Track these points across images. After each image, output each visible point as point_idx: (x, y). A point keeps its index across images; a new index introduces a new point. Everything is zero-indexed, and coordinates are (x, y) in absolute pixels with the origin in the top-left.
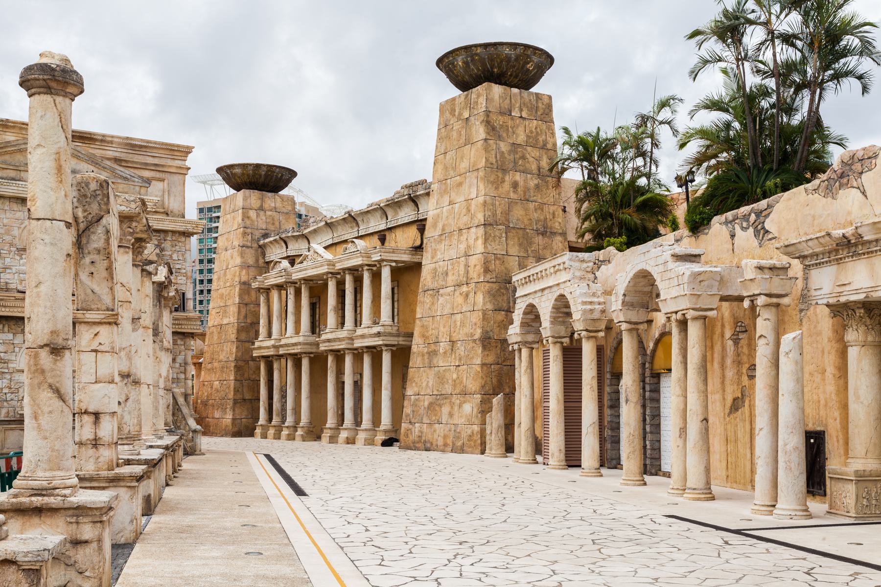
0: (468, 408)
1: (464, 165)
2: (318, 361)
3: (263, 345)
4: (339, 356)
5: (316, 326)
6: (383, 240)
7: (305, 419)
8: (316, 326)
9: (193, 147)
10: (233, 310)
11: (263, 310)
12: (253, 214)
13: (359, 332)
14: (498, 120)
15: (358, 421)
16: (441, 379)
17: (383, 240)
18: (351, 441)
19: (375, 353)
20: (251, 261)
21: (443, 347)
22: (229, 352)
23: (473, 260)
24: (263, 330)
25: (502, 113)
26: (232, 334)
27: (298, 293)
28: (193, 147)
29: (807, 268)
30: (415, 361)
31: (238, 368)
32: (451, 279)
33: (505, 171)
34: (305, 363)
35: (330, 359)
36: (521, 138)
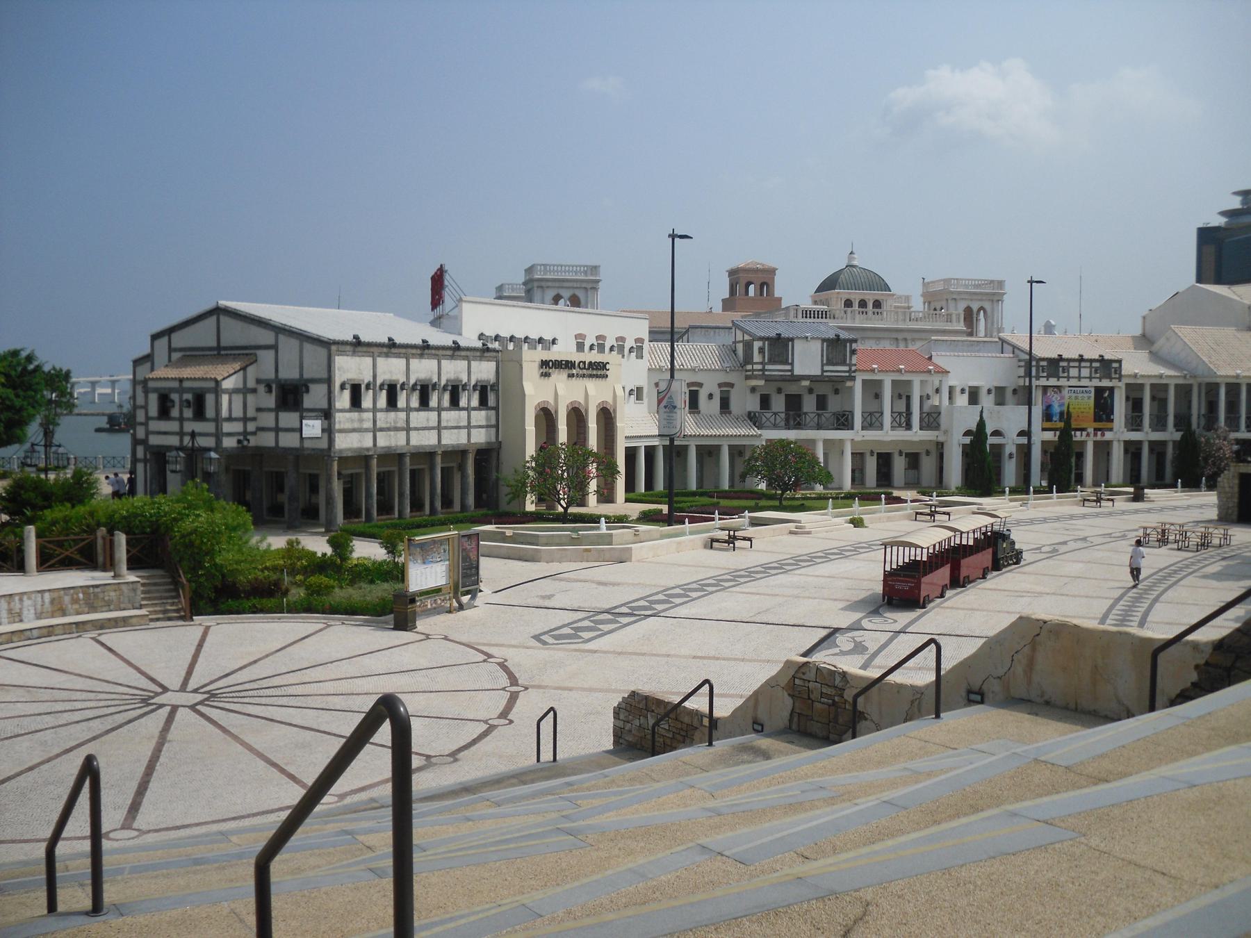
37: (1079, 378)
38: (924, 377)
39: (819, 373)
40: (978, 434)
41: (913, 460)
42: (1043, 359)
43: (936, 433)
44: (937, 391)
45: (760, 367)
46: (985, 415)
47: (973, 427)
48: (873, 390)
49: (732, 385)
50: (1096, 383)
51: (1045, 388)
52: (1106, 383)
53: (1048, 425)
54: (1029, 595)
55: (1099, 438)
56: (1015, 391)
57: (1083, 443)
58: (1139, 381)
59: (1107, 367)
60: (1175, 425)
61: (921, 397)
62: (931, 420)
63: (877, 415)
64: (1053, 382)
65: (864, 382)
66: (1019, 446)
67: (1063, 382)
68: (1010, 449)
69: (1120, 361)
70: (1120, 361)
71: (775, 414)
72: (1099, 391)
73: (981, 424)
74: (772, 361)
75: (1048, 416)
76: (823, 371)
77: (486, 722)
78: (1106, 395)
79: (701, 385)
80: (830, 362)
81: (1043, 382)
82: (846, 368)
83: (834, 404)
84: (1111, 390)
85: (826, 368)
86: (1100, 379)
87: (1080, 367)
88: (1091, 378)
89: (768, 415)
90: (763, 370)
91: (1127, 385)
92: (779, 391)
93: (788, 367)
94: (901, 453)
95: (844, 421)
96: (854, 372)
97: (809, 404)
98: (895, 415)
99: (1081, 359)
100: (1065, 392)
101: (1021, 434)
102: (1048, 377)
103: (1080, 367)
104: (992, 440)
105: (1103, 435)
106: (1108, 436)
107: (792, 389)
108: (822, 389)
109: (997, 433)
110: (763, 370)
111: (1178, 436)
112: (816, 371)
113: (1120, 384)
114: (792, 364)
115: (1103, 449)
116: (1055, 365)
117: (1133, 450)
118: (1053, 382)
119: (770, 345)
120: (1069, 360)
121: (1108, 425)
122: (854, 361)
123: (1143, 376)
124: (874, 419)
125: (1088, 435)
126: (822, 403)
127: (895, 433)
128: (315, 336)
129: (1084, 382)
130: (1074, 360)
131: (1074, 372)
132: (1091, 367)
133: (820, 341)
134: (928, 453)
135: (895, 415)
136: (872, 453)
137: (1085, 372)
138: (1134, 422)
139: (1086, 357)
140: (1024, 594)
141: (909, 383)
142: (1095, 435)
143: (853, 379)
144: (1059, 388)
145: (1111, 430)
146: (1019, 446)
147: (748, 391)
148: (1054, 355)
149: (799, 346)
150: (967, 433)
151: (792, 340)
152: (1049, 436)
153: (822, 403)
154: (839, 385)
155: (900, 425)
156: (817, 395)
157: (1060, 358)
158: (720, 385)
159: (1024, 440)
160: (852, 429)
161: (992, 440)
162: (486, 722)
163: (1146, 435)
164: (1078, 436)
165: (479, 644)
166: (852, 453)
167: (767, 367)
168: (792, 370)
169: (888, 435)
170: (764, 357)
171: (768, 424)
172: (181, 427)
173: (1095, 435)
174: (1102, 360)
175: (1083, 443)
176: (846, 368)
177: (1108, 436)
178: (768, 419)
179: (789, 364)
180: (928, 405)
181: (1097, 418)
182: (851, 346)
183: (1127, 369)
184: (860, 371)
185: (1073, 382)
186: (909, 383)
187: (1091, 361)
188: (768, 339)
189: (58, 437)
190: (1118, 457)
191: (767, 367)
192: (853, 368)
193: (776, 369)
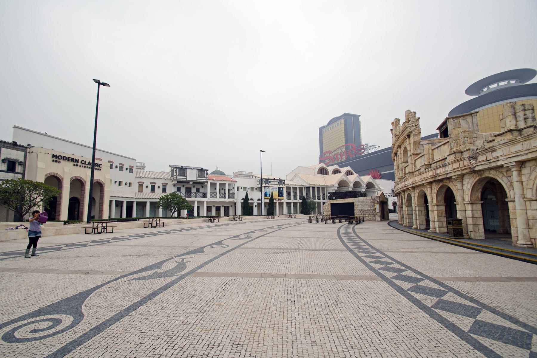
9: (360, 116)
28: (360, 116)
37: (274, 184)
38: (230, 183)
40: (246, 199)
41: (227, 209)
43: (233, 199)
44: (234, 188)
45: (175, 177)
46: (248, 193)
47: (244, 197)
48: (213, 185)
49: (167, 184)
50: (279, 186)
51: (265, 187)
52: (281, 186)
53: (266, 197)
54: (282, 251)
55: (280, 201)
57: (276, 203)
58: (290, 186)
59: (281, 181)
60: (300, 198)
61: (229, 190)
62: (232, 195)
63: (215, 194)
64: (267, 185)
66: (258, 203)
67: (269, 185)
68: (256, 204)
69: (284, 180)
70: (284, 180)
71: (201, 193)
72: (279, 188)
73: (247, 196)
74: (179, 175)
75: (266, 195)
76: (197, 179)
78: (281, 189)
79: (155, 183)
80: (199, 176)
82: (205, 179)
83: (202, 190)
84: (283, 188)
85: (198, 178)
86: (280, 185)
87: (274, 182)
88: (277, 185)
89: (199, 193)
90: (176, 178)
91: (287, 187)
92: (183, 186)
93: (186, 177)
94: (223, 206)
95: (205, 195)
96: (208, 180)
97: (194, 190)
98: (211, 194)
99: (274, 179)
101: (259, 200)
102: (265, 184)
103: (274, 182)
104: (250, 201)
105: (281, 201)
106: (282, 201)
107: (188, 186)
109: (251, 199)
110: (176, 178)
111: (301, 201)
112: (195, 179)
113: (285, 187)
114: (186, 176)
115: (281, 204)
116: (267, 180)
117: (289, 204)
119: (179, 170)
120: (271, 179)
121: (282, 198)
122: (207, 177)
123: (291, 185)
124: (214, 195)
125: (277, 200)
126: (198, 190)
127: (221, 199)
128: (80, 210)
130: (272, 179)
131: (272, 183)
132: (277, 182)
133: (196, 170)
134: (231, 206)
135: (211, 194)
136: (214, 206)
137: (276, 183)
138: (289, 197)
139: (276, 179)
140: (278, 251)
141: (225, 184)
142: (279, 201)
143: (207, 182)
145: (282, 199)
146: (258, 203)
147: (173, 186)
148: (267, 178)
150: (242, 199)
151: (187, 169)
152: (267, 201)
153: (198, 190)
154: (202, 184)
155: (222, 197)
156: (186, 188)
157: (269, 179)
158: (162, 184)
159: (260, 202)
160: (207, 197)
161: (250, 201)
163: (292, 201)
164: (275, 201)
166: (207, 206)
167: (178, 177)
168: (186, 179)
169: (218, 199)
171: (199, 196)
173: (279, 201)
174: (280, 180)
175: (276, 203)
176: (205, 179)
177: (282, 201)
178: (183, 194)
179: (185, 176)
180: (231, 192)
181: (279, 196)
182: (206, 172)
183: (286, 182)
184: (209, 180)
186: (225, 184)
187: (277, 180)
188: (178, 168)
189: (529, 189)
190: (285, 205)
191: (178, 177)
192: (207, 179)
193: (181, 178)
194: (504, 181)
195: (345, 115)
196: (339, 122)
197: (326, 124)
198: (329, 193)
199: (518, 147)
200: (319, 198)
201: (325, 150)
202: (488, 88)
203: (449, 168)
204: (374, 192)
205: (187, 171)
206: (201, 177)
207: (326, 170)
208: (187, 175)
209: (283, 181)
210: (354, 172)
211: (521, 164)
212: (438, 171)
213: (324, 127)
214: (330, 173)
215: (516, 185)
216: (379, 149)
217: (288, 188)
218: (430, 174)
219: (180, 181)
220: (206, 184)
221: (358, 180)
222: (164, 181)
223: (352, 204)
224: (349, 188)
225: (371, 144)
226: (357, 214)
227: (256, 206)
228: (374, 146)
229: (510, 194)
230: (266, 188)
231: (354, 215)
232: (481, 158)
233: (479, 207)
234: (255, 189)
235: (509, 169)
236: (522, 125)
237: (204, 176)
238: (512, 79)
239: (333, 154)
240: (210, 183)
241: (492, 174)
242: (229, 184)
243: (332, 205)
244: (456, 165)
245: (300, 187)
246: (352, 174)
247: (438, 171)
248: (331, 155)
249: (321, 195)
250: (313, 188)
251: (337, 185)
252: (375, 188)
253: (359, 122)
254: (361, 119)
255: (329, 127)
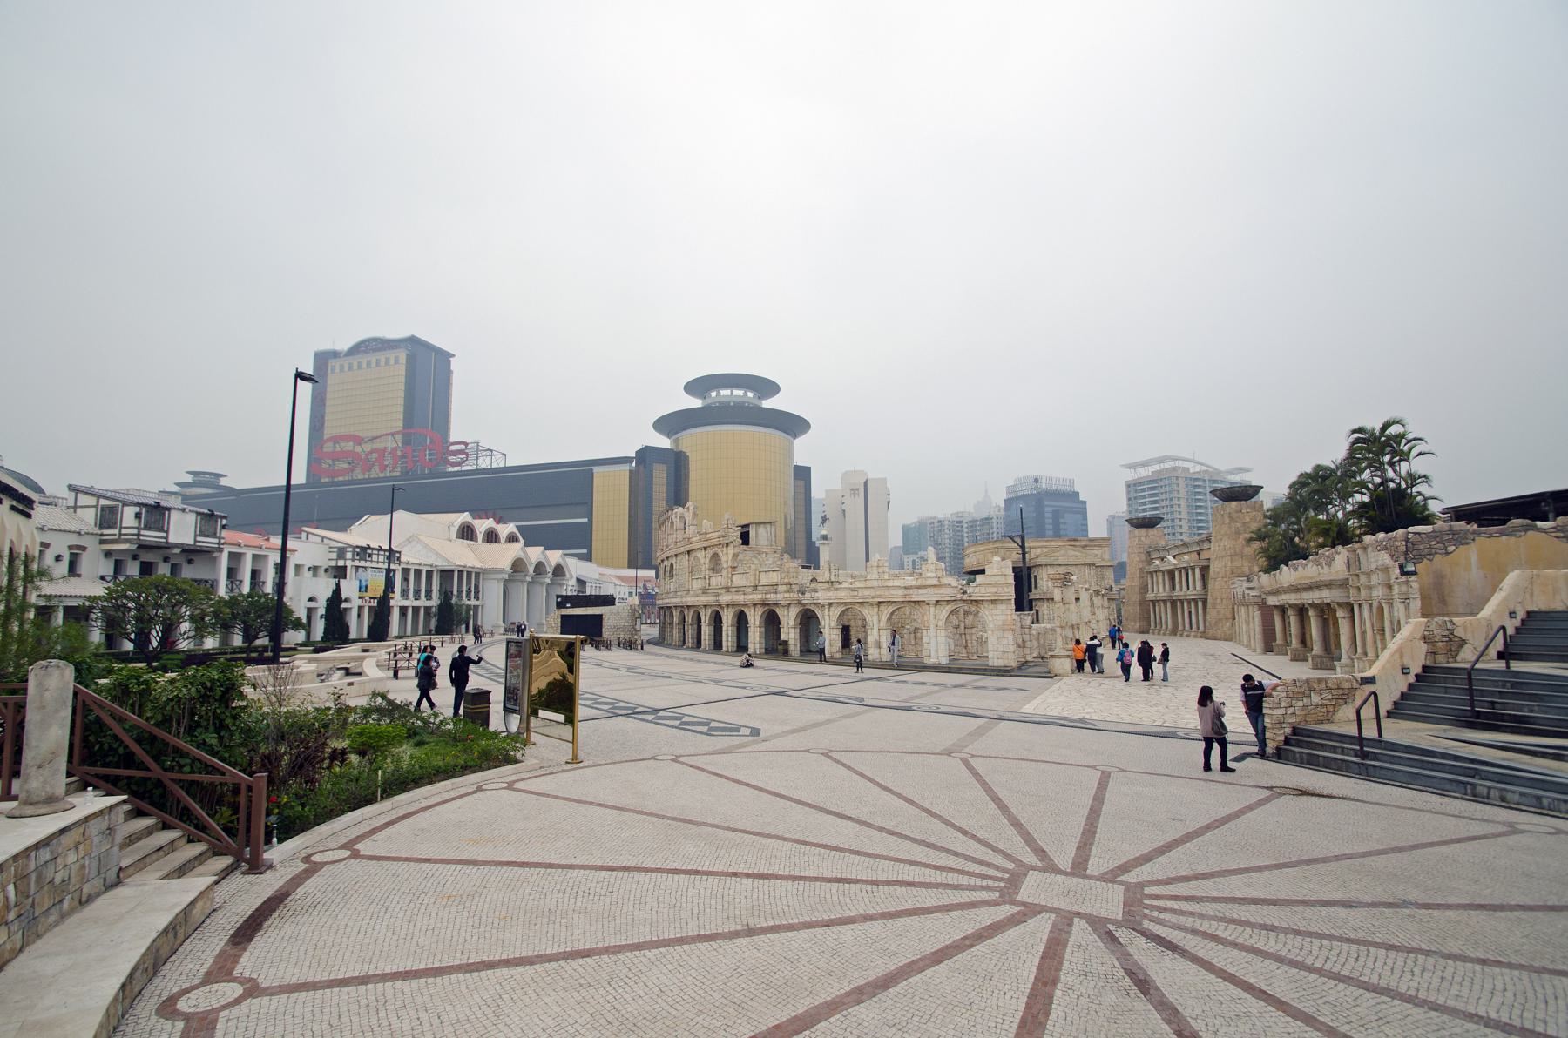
0: (1228, 624)
1: (1222, 532)
2: (1174, 603)
3: (1150, 595)
4: (1182, 602)
5: (1173, 588)
6: (1199, 554)
7: (1170, 626)
8: (1173, 588)
9: (453, 356)
10: (1136, 580)
11: (1150, 581)
12: (1143, 539)
13: (1189, 593)
14: (1235, 515)
15: (1181, 587)
16: (1218, 613)
17: (1199, 554)
18: (1188, 636)
19: (1195, 601)
20: (1144, 558)
21: (1218, 601)
22: (1136, 597)
23: (1228, 569)
24: (1150, 589)
25: (1237, 512)
26: (1137, 590)
27: (1180, 572)
28: (453, 356)
29: (123, 506)
30: (1209, 606)
31: (1140, 605)
32: (1220, 575)
33: (1240, 534)
34: (1169, 604)
35: (1178, 603)
36: (1248, 520)
37: (378, 562)
39: (192, 542)
42: (357, 547)
49: (84, 549)
51: (357, 567)
56: (326, 570)
64: (362, 563)
65: (230, 554)
69: (400, 553)
70: (400, 553)
74: (147, 527)
76: (196, 541)
77: (253, 990)
80: (202, 534)
81: (357, 563)
85: (199, 539)
90: (138, 535)
93: (164, 535)
100: (369, 570)
108: (148, 557)
109: (346, 600)
110: (138, 535)
112: (188, 540)
114: (167, 532)
117: (403, 610)
118: (362, 563)
119: (147, 512)
122: (223, 535)
129: (381, 565)
130: (375, 549)
131: (375, 558)
143: (221, 550)
144: (365, 568)
147: (102, 556)
148: (364, 545)
149: (175, 516)
151: (169, 509)
156: (142, 562)
162: (253, 990)
163: (410, 602)
165: (1487, 636)
167: (143, 532)
168: (166, 538)
170: (140, 522)
172: (98, 502)
176: (216, 541)
183: (403, 559)
185: (374, 565)
188: (146, 505)
191: (143, 532)
192: (222, 541)
193: (151, 536)
194: (819, 614)
195: (413, 341)
196: (391, 355)
197: (344, 345)
198: (558, 597)
199: (831, 594)
200: (469, 598)
201: (329, 432)
202: (718, 394)
203: (780, 596)
204: (562, 585)
205: (169, 516)
206: (208, 536)
207: (472, 530)
208: (168, 528)
209: (398, 555)
210: (521, 538)
211: (831, 604)
212: (768, 596)
213: (335, 354)
214: (480, 537)
215: (827, 617)
216: (502, 465)
217: (406, 571)
218: (759, 596)
219: (147, 543)
220: (215, 555)
221: (522, 555)
222: (75, 541)
223: (600, 616)
224: (526, 575)
225: (484, 444)
226: (607, 633)
227: (321, 617)
228: (491, 451)
229: (822, 622)
230: (360, 569)
231: (600, 634)
232: (807, 595)
233: (798, 630)
234: (322, 571)
235: (823, 606)
236: (833, 579)
237: (215, 533)
238: (739, 386)
239: (368, 447)
240: (230, 553)
241: (812, 607)
242: (255, 557)
243: (563, 617)
244: (787, 595)
245: (417, 567)
246: (517, 540)
247: (768, 596)
248: (358, 449)
249: (465, 588)
250: (460, 572)
251: (508, 569)
252: (565, 576)
253: (448, 373)
254: (455, 365)
255: (355, 360)
